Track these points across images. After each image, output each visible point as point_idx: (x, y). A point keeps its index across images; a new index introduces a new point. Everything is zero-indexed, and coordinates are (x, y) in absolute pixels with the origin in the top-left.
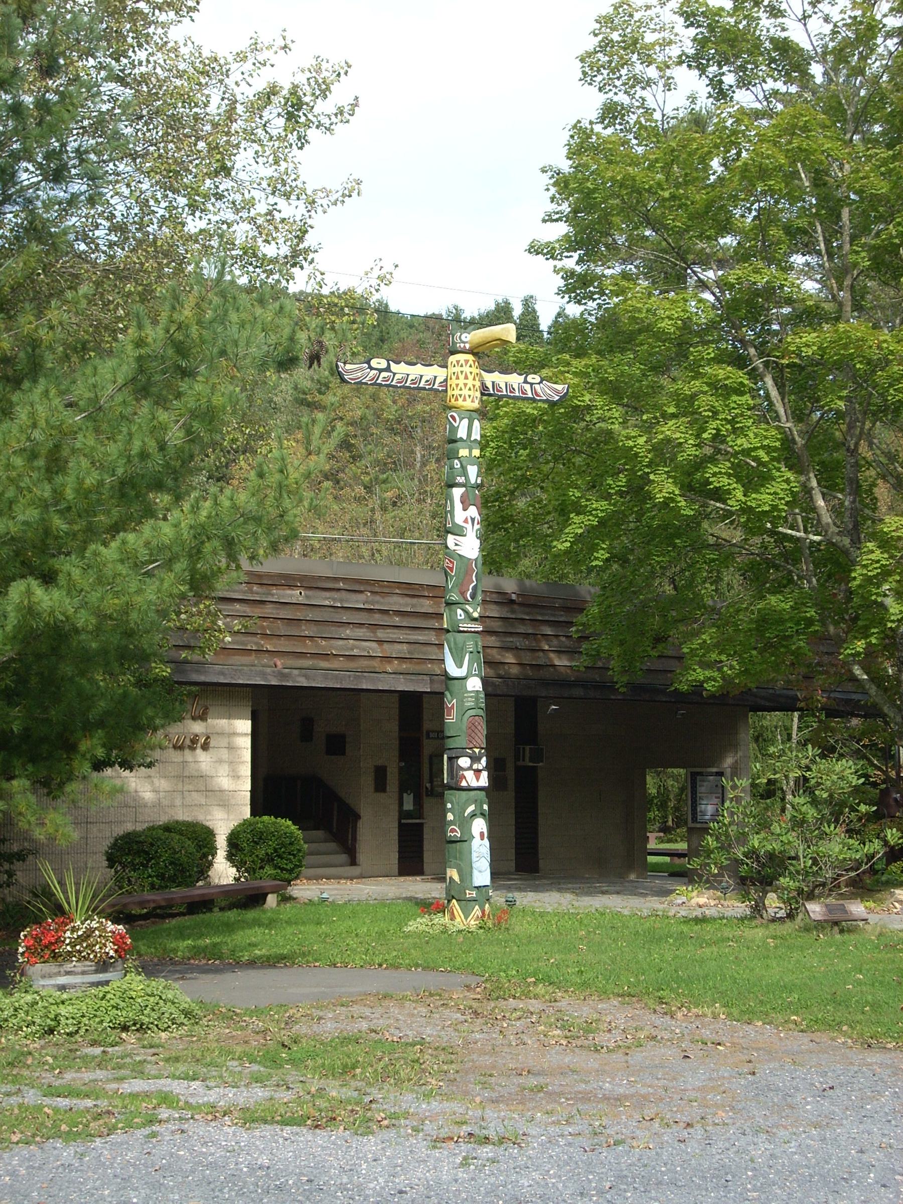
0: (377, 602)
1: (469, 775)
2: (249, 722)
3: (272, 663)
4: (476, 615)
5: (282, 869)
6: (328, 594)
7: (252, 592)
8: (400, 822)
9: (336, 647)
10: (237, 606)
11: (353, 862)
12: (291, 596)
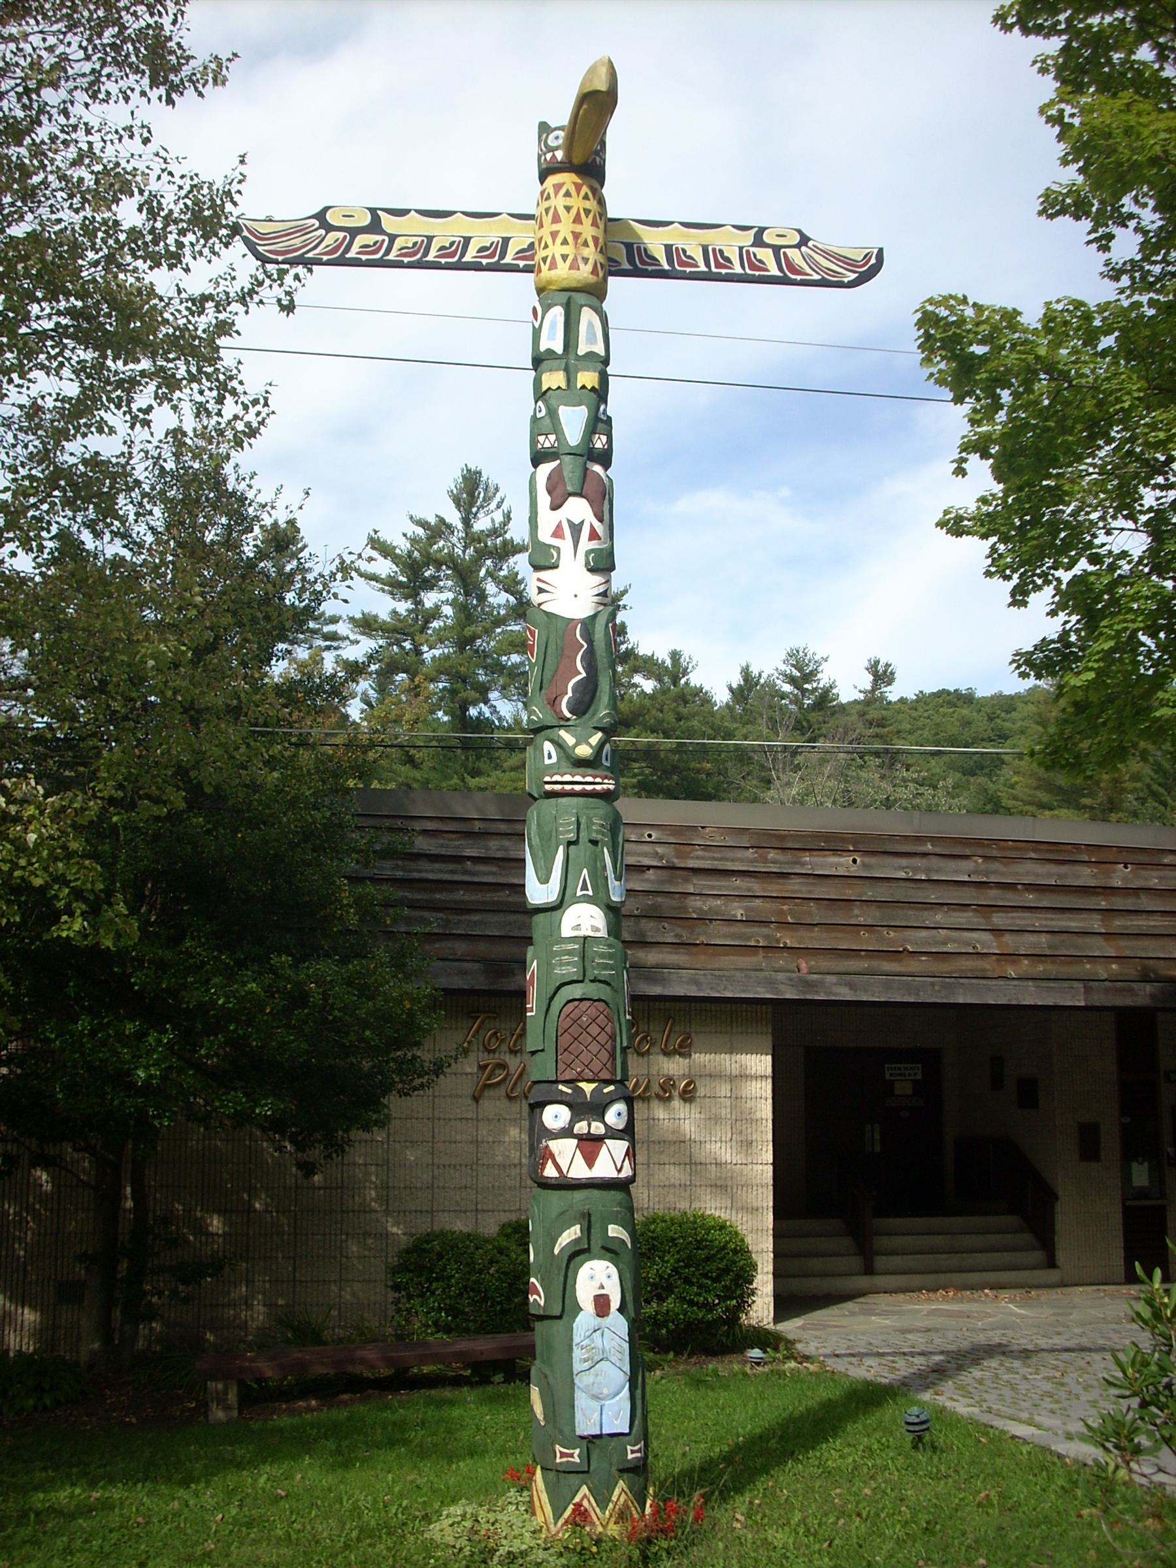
0: (994, 872)
1: (565, 1151)
2: (769, 1058)
3: (793, 966)
4: (584, 751)
5: (691, 1303)
6: (904, 862)
7: (766, 861)
8: (1124, 1204)
9: (915, 940)
10: (738, 882)
11: (1051, 1263)
12: (837, 865)
